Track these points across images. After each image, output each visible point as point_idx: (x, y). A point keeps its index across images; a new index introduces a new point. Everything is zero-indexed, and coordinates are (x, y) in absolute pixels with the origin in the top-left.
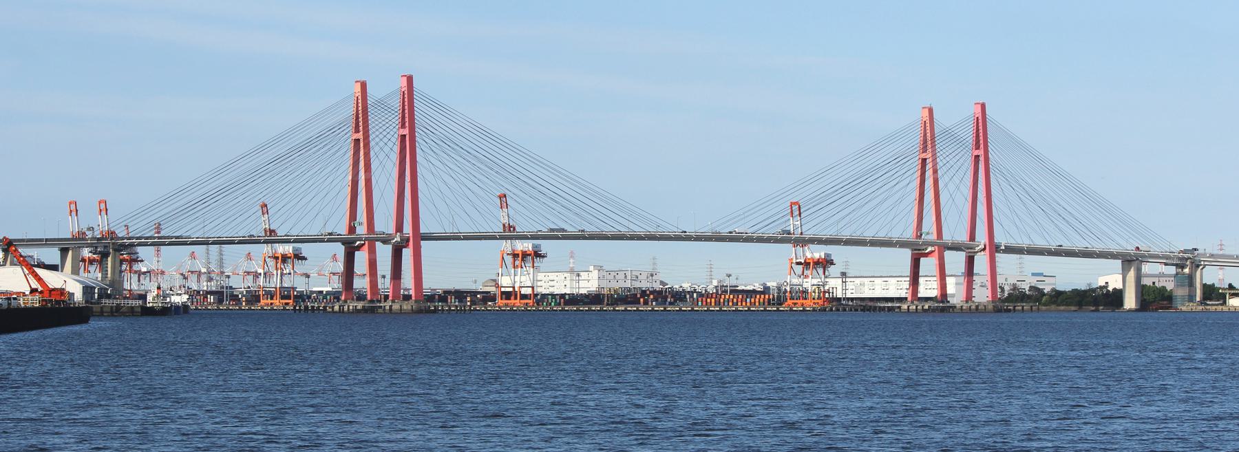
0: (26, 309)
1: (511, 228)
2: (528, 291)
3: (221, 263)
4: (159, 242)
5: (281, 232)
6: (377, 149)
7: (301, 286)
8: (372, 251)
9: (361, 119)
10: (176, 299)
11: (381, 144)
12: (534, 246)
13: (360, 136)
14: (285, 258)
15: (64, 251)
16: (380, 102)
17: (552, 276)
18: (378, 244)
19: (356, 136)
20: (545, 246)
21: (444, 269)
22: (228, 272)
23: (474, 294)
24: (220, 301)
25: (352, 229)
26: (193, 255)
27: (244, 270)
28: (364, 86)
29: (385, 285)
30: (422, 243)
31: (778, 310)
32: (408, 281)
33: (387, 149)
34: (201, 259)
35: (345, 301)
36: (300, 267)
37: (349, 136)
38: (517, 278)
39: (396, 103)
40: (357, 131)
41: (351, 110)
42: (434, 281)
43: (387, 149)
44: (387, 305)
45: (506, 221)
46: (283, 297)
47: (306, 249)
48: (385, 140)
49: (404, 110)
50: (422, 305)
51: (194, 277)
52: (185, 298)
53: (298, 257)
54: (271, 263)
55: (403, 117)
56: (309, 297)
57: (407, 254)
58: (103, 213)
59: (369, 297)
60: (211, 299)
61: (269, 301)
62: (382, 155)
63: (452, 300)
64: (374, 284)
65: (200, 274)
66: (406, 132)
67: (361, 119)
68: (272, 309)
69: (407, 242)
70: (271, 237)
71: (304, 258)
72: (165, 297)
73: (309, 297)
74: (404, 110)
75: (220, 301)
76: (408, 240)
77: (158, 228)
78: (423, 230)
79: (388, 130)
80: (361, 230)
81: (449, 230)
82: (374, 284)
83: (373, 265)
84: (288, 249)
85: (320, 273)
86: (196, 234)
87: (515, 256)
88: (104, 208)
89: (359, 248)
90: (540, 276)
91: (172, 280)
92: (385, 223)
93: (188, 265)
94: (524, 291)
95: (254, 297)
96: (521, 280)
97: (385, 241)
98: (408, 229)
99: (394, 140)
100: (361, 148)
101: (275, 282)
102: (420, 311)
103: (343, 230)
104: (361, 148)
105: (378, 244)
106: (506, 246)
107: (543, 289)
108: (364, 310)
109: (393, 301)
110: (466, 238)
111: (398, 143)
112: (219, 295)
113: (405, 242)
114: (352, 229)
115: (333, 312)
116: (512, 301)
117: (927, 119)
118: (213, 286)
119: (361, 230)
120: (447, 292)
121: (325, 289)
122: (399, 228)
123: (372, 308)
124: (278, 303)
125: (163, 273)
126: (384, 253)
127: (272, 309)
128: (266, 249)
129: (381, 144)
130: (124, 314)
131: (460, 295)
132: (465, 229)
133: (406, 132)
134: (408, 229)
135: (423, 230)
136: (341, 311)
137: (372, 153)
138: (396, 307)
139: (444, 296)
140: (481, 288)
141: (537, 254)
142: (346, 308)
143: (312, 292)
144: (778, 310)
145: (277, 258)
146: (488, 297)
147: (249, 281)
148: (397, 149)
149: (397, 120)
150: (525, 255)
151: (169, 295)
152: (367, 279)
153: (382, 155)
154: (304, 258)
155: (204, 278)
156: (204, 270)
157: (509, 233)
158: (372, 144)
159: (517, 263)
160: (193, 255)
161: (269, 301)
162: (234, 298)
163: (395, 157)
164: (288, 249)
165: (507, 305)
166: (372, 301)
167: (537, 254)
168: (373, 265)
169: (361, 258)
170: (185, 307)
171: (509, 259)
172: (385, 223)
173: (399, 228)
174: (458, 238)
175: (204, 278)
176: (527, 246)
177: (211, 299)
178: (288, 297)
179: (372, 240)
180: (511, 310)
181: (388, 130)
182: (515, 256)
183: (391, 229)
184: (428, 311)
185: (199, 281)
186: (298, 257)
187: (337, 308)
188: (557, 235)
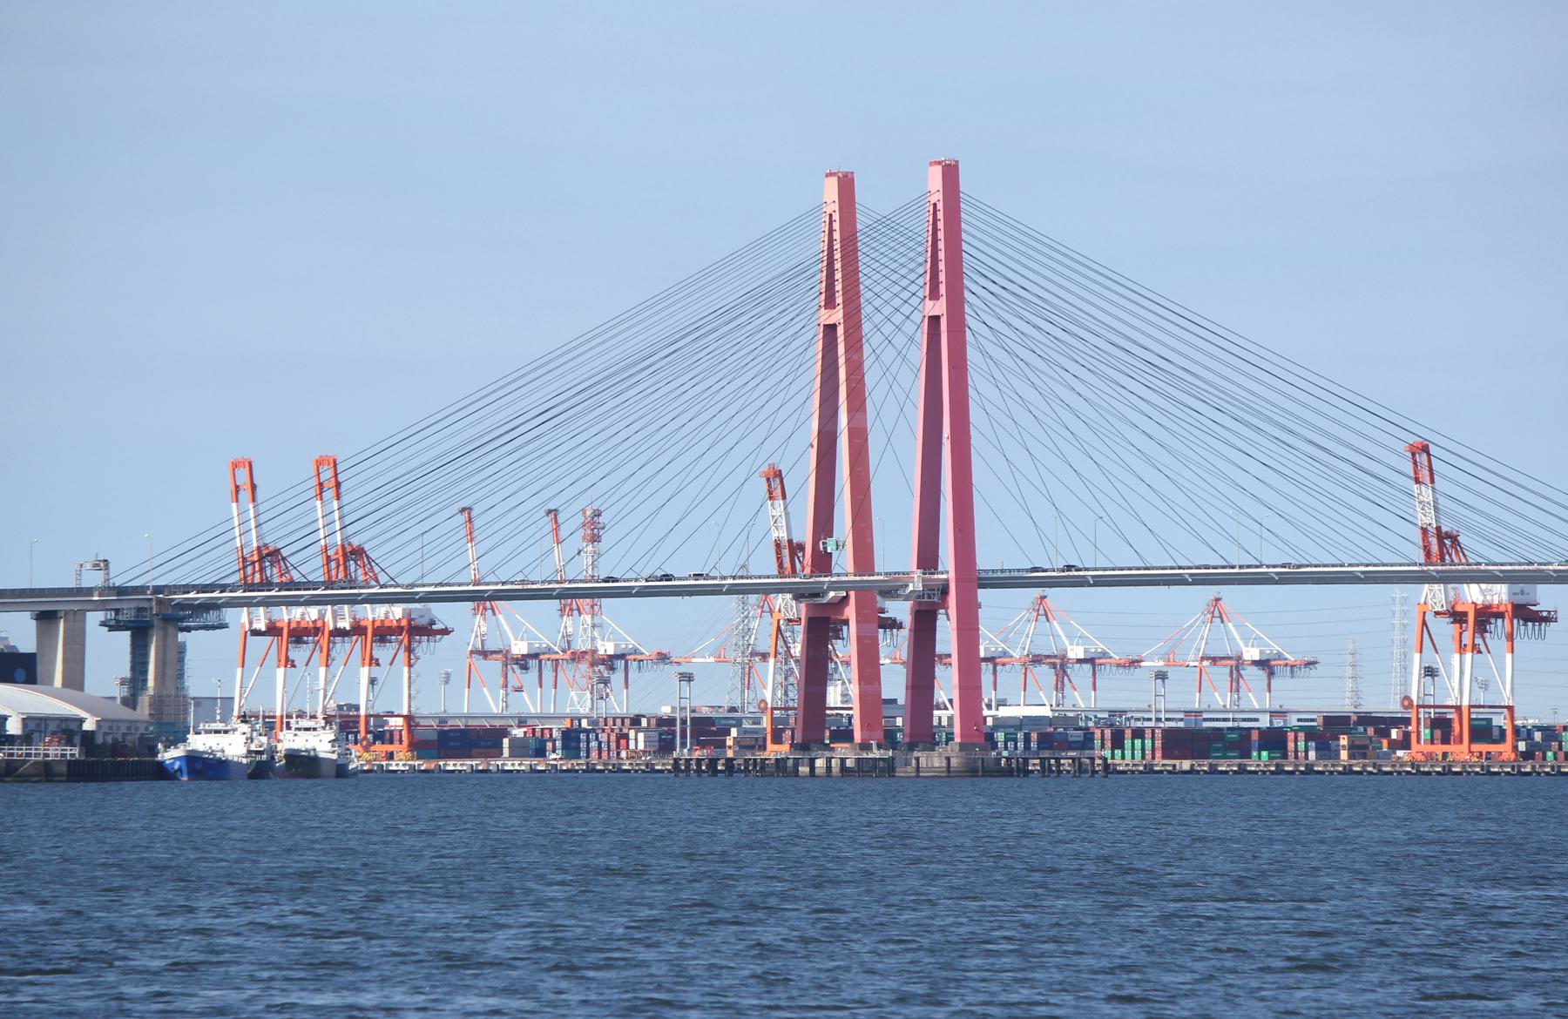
15: (46, 618)
16: (884, 223)
28: (846, 186)
30: (983, 595)
31: (1242, 770)
33: (900, 340)
40: (830, 303)
42: (1019, 701)
43: (900, 340)
45: (1429, 519)
47: (443, 613)
58: (329, 494)
60: (639, 741)
62: (889, 355)
75: (665, 746)
76: (945, 591)
78: (987, 559)
79: (901, 304)
88: (329, 480)
99: (909, 328)
110: (1100, 582)
130: (25, 778)
133: (939, 308)
144: (1242, 770)
150: (1485, 616)
153: (889, 355)
167: (1525, 613)
173: (928, 559)
180: (1448, 772)
181: (901, 304)
185: (1235, 687)
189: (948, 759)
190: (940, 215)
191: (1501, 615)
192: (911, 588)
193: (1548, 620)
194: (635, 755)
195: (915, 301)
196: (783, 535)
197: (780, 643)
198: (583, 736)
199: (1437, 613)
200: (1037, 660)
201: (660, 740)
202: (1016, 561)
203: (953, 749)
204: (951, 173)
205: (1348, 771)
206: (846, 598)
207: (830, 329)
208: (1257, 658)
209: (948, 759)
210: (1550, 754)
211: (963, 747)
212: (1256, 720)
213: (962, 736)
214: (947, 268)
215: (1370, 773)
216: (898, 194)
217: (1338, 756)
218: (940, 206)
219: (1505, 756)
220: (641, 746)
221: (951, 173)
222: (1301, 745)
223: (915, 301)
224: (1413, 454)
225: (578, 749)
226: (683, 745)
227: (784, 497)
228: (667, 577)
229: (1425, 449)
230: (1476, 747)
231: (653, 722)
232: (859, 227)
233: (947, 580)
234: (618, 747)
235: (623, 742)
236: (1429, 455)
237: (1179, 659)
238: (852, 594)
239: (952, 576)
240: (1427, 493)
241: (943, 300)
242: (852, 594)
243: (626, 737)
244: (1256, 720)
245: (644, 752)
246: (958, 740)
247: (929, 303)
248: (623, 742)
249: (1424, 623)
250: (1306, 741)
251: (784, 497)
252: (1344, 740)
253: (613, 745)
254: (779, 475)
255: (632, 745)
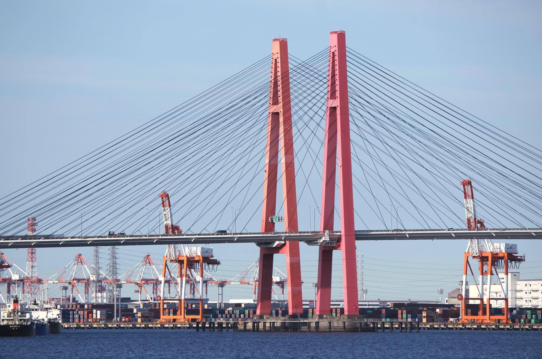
0: (3, 325)
1: (175, 229)
2: (501, 304)
3: (114, 269)
4: (32, 243)
5: (491, 225)
6: (300, 124)
7: (214, 298)
8: (295, 253)
9: (281, 87)
10: (40, 316)
11: (306, 118)
12: (507, 247)
13: (279, 108)
14: (191, 262)
16: (303, 65)
17: (536, 285)
18: (302, 245)
19: (274, 109)
20: (523, 247)
21: (389, 276)
22: (122, 277)
23: (431, 307)
24: (109, 317)
25: (269, 226)
26: (79, 259)
27: (143, 277)
28: (284, 45)
29: (310, 293)
30: (358, 243)
32: (338, 291)
33: (312, 125)
34: (88, 264)
35: (261, 317)
36: (209, 272)
37: (265, 109)
38: (486, 287)
39: (325, 68)
41: (268, 77)
43: (312, 125)
44: (313, 321)
46: (189, 312)
48: (311, 113)
49: (333, 76)
50: (357, 321)
51: (81, 287)
52: (55, 314)
53: (209, 260)
54: (175, 267)
55: (333, 84)
56: (222, 312)
57: (338, 257)
59: (290, 312)
60: (97, 314)
61: (172, 317)
62: (306, 133)
63: (404, 317)
64: (297, 295)
65: (88, 282)
66: (336, 103)
67: (281, 87)
68: (175, 327)
69: (338, 242)
70: (173, 236)
71: (216, 262)
72: (23, 313)
73: (222, 312)
74: (333, 76)
75: (109, 317)
76: (339, 240)
77: (33, 225)
78: (358, 226)
79: (314, 100)
80: (281, 227)
81: (392, 226)
82: (297, 295)
83: (295, 269)
84: (196, 250)
85: (234, 281)
86: (72, 232)
87: (483, 259)
89: (278, 249)
90: (521, 285)
91: (51, 289)
92: (310, 220)
93: (74, 272)
94: (495, 304)
95: (152, 312)
96: (494, 290)
97: (311, 241)
98: (339, 225)
99: (321, 113)
100: (281, 124)
101: (181, 292)
102: (354, 330)
103: (257, 227)
104: (281, 124)
105: (302, 245)
106: (471, 246)
107: (524, 301)
108: (285, 327)
109: (321, 317)
111: (327, 118)
112: (108, 310)
113: (335, 242)
114: (269, 226)
115: (245, 330)
116: (480, 317)
117: (335, 49)
118: (102, 298)
119: (281, 227)
120: (398, 305)
121: (244, 301)
122: (328, 224)
123: (295, 322)
124: (182, 319)
125: (40, 281)
126: (310, 256)
127: (175, 327)
128: (167, 250)
129: (306, 118)
131: (414, 309)
132: (411, 225)
133: (336, 103)
134: (339, 225)
135: (358, 226)
136: (255, 329)
137: (294, 130)
138: (324, 324)
139: (392, 311)
140: (444, 300)
141: (512, 257)
142: (261, 326)
143: (227, 305)
145: (181, 262)
146: (450, 311)
147: (148, 294)
148: (325, 124)
149: (325, 89)
150: (496, 258)
151: (29, 310)
152: (288, 288)
153: (306, 133)
154: (216, 262)
155: (93, 288)
156: (93, 278)
157: (476, 230)
158: (294, 118)
159: (486, 268)
160: (79, 259)
161: (172, 317)
162: (128, 313)
163: (323, 134)
164: (195, 251)
165: (473, 322)
166: (294, 316)
167: (512, 257)
168: (295, 269)
169: (281, 264)
170: (53, 324)
171: (475, 264)
172: (310, 220)
173: (328, 224)
174: (402, 237)
175: (93, 288)
176: (499, 246)
177: (97, 314)
178: (196, 312)
179: (294, 241)
180: (479, 328)
181: (314, 100)
182: (483, 259)
183: (319, 226)
184: (366, 329)
185: (87, 292)
186: (209, 260)
187: (250, 325)
188: (223, 238)
189: (344, 323)
190: (336, 58)
191: (502, 258)
192: (323, 239)
193: (520, 260)
194: (96, 321)
195: (323, 101)
196: (169, 222)
197: (167, 270)
198: (71, 312)
199: (474, 257)
200: (147, 281)
201: (107, 314)
202: (337, 230)
203: (345, 318)
204: (341, 37)
205: (119, 327)
206: (285, 243)
207: (275, 115)
208: (278, 280)
209: (344, 323)
210: (522, 320)
211: (349, 317)
212: (339, 305)
213: (349, 311)
214: (339, 82)
215: (443, 329)
216: (310, 50)
217: (137, 320)
218: (336, 53)
219: (181, 321)
220: (99, 317)
221: (341, 37)
222: (404, 316)
223: (323, 101)
224: (464, 186)
225: (69, 318)
226: (117, 316)
227: (170, 206)
228: (224, 232)
229: (470, 183)
230: (492, 317)
231: (90, 306)
232: (290, 66)
233: (340, 235)
234: (88, 317)
235: (90, 315)
236: (471, 187)
237: (246, 280)
238: (288, 242)
239: (343, 233)
240: (470, 203)
241: (338, 100)
242: (288, 242)
243: (92, 313)
244: (339, 305)
245: (100, 320)
246: (346, 313)
247: (331, 101)
248: (90, 315)
249: (468, 262)
250: (407, 314)
251: (170, 206)
252: (424, 314)
253: (86, 316)
254: (167, 196)
255: (94, 316)
